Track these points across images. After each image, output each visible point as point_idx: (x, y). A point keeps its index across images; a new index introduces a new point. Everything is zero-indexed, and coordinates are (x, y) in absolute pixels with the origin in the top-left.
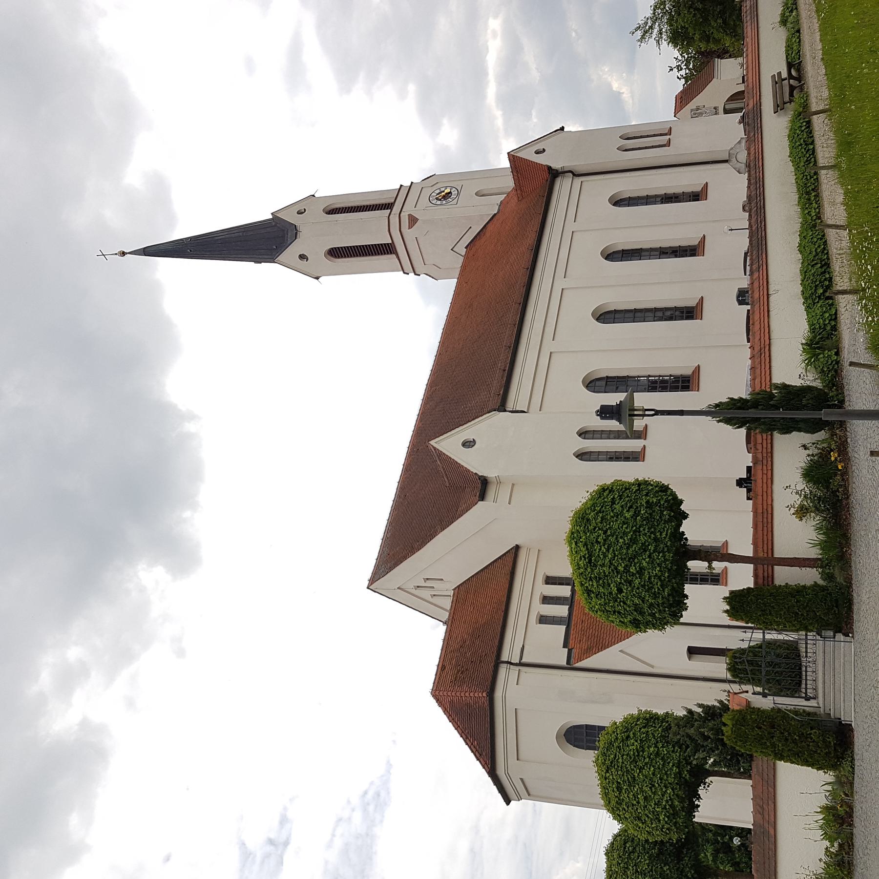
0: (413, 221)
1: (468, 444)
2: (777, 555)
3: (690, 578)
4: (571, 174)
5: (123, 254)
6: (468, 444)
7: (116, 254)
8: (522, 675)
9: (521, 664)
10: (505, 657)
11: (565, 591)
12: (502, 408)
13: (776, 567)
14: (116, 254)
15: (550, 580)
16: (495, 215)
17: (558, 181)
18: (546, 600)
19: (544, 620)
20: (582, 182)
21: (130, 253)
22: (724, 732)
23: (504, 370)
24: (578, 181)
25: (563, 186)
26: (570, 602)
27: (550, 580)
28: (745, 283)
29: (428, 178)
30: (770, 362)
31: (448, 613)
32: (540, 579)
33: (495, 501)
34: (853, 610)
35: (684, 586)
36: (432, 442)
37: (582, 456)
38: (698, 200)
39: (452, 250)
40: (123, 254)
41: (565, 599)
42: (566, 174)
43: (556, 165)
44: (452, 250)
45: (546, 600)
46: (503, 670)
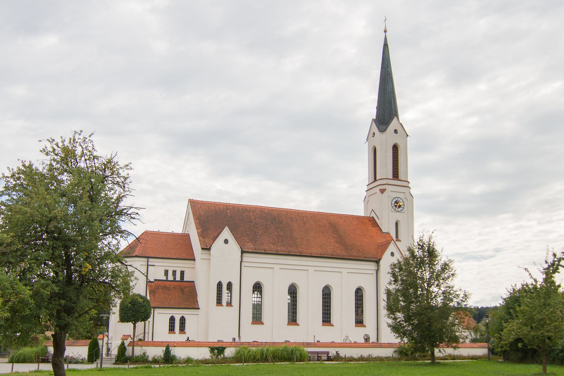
0: (382, 191)
1: (226, 241)
2: (135, 347)
3: (294, 312)
4: (377, 269)
5: (385, 32)
6: (226, 241)
7: (385, 28)
8: (144, 267)
9: (148, 265)
10: (150, 260)
11: (178, 278)
12: (243, 252)
13: (132, 347)
14: (385, 28)
15: (182, 273)
16: (381, 230)
17: (374, 264)
18: (174, 272)
19: (166, 272)
20: (373, 274)
21: (386, 35)
22: (512, 313)
23: (265, 250)
24: (374, 272)
25: (372, 266)
26: (175, 280)
27: (182, 273)
28: (320, 342)
29: (411, 195)
30: (81, 346)
31: (181, 233)
32: (182, 269)
33: (202, 254)
34: (123, 365)
35: (143, 321)
36: (227, 227)
37: (220, 285)
38: (356, 323)
39: (373, 210)
40: (385, 32)
41: (175, 279)
42: (377, 267)
43: (381, 263)
44: (373, 210)
45: (174, 272)
46: (146, 260)
